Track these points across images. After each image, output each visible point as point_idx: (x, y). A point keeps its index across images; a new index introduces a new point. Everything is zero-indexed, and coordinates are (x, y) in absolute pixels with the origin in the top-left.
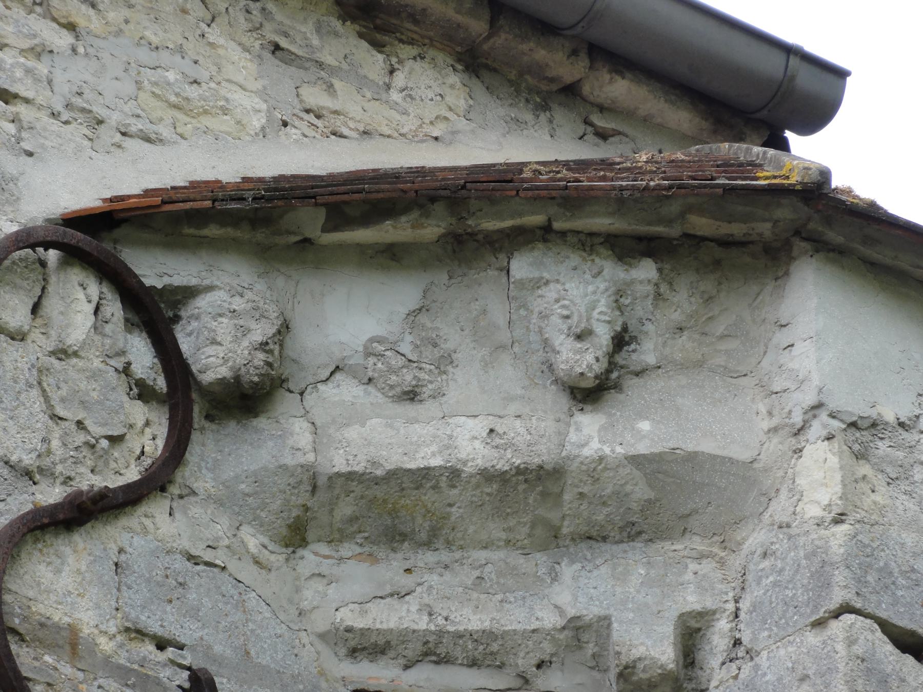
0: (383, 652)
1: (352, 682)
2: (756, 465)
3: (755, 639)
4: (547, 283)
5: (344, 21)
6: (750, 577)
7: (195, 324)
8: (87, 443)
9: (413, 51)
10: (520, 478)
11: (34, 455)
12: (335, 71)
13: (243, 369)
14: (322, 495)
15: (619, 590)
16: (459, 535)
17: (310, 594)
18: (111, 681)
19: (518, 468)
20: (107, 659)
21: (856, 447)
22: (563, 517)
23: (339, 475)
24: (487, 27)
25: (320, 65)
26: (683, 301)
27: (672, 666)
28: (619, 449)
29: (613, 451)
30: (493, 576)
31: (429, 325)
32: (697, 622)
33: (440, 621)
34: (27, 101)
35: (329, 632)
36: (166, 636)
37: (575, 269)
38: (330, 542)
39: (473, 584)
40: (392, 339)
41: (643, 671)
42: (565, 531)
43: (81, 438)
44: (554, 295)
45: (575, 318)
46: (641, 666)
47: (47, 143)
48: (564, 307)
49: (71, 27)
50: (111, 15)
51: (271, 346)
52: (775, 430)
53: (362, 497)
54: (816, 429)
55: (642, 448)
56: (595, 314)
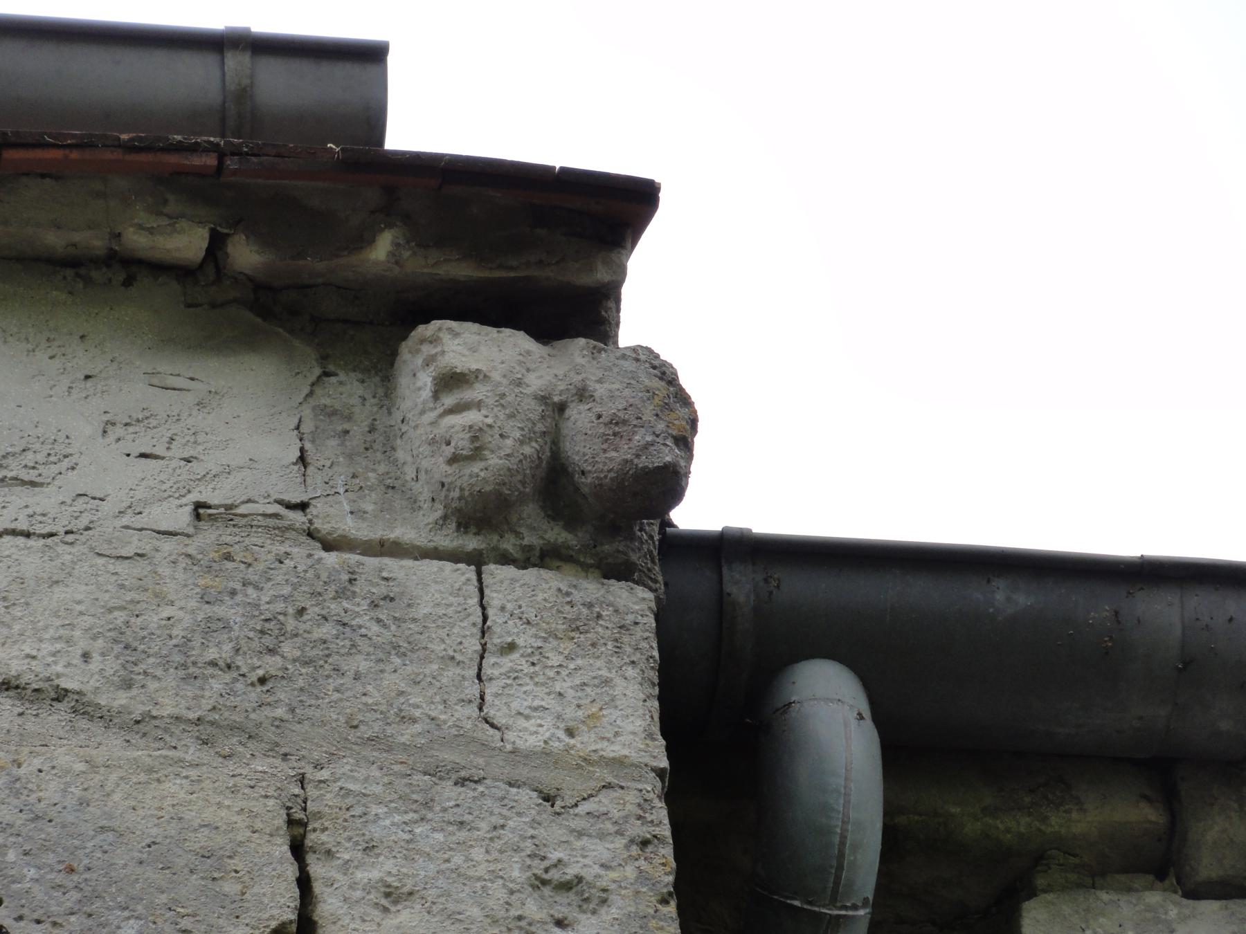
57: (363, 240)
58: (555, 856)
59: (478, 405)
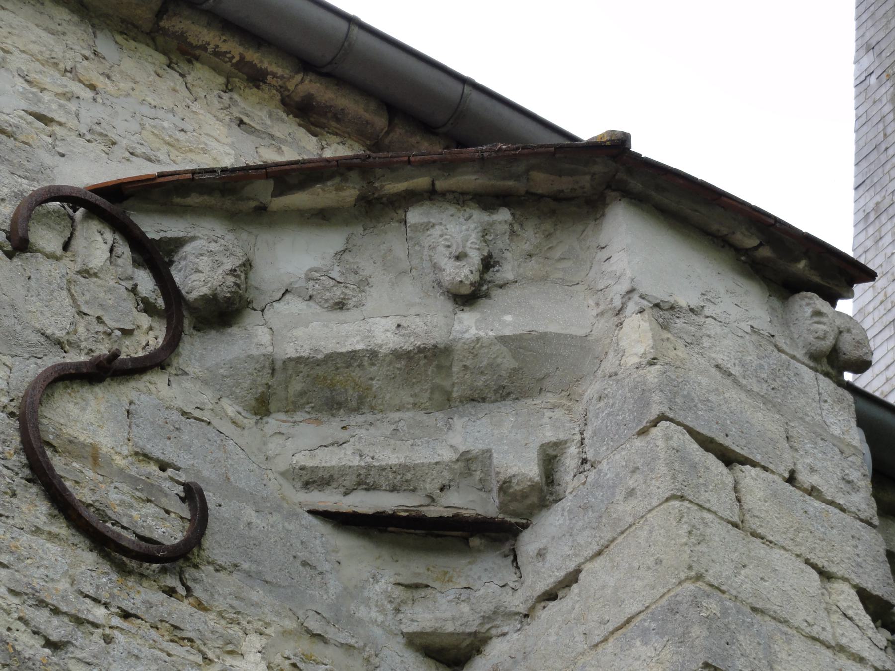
0: (328, 483)
1: (306, 505)
2: (589, 338)
3: (597, 453)
4: (433, 226)
5: (288, 115)
6: (590, 415)
7: (183, 263)
8: (105, 332)
9: (338, 139)
10: (422, 355)
11: (64, 332)
12: (283, 141)
13: (219, 289)
14: (280, 376)
15: (496, 432)
16: (380, 401)
17: (273, 446)
18: (124, 485)
19: (419, 347)
20: (121, 471)
21: (661, 320)
22: (453, 385)
23: (290, 359)
24: (387, 123)
25: (272, 137)
26: (530, 236)
27: (537, 479)
28: (490, 333)
29: (486, 334)
30: (405, 428)
31: (351, 260)
32: (554, 450)
33: (369, 460)
34: (60, 124)
35: (288, 471)
36: (166, 460)
37: (452, 215)
38: (287, 412)
39: (392, 434)
40: (324, 269)
41: (517, 484)
42: (455, 395)
43: (101, 328)
44: (439, 232)
45: (455, 247)
46: (515, 481)
47: (75, 150)
48: (446, 239)
49: (93, 87)
50: (122, 85)
51: (239, 272)
52: (602, 314)
53: (308, 376)
54: (632, 307)
55: (508, 332)
56: (469, 244)
57: (797, 261)
58: (847, 471)
59: (825, 324)
